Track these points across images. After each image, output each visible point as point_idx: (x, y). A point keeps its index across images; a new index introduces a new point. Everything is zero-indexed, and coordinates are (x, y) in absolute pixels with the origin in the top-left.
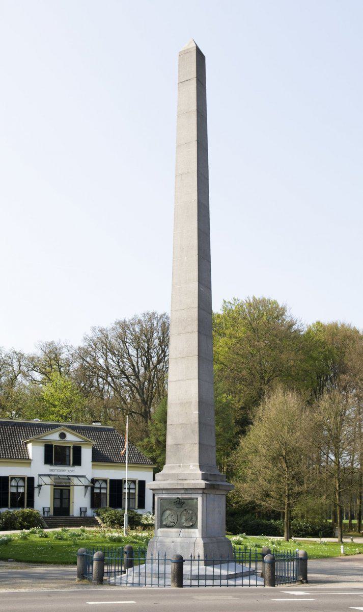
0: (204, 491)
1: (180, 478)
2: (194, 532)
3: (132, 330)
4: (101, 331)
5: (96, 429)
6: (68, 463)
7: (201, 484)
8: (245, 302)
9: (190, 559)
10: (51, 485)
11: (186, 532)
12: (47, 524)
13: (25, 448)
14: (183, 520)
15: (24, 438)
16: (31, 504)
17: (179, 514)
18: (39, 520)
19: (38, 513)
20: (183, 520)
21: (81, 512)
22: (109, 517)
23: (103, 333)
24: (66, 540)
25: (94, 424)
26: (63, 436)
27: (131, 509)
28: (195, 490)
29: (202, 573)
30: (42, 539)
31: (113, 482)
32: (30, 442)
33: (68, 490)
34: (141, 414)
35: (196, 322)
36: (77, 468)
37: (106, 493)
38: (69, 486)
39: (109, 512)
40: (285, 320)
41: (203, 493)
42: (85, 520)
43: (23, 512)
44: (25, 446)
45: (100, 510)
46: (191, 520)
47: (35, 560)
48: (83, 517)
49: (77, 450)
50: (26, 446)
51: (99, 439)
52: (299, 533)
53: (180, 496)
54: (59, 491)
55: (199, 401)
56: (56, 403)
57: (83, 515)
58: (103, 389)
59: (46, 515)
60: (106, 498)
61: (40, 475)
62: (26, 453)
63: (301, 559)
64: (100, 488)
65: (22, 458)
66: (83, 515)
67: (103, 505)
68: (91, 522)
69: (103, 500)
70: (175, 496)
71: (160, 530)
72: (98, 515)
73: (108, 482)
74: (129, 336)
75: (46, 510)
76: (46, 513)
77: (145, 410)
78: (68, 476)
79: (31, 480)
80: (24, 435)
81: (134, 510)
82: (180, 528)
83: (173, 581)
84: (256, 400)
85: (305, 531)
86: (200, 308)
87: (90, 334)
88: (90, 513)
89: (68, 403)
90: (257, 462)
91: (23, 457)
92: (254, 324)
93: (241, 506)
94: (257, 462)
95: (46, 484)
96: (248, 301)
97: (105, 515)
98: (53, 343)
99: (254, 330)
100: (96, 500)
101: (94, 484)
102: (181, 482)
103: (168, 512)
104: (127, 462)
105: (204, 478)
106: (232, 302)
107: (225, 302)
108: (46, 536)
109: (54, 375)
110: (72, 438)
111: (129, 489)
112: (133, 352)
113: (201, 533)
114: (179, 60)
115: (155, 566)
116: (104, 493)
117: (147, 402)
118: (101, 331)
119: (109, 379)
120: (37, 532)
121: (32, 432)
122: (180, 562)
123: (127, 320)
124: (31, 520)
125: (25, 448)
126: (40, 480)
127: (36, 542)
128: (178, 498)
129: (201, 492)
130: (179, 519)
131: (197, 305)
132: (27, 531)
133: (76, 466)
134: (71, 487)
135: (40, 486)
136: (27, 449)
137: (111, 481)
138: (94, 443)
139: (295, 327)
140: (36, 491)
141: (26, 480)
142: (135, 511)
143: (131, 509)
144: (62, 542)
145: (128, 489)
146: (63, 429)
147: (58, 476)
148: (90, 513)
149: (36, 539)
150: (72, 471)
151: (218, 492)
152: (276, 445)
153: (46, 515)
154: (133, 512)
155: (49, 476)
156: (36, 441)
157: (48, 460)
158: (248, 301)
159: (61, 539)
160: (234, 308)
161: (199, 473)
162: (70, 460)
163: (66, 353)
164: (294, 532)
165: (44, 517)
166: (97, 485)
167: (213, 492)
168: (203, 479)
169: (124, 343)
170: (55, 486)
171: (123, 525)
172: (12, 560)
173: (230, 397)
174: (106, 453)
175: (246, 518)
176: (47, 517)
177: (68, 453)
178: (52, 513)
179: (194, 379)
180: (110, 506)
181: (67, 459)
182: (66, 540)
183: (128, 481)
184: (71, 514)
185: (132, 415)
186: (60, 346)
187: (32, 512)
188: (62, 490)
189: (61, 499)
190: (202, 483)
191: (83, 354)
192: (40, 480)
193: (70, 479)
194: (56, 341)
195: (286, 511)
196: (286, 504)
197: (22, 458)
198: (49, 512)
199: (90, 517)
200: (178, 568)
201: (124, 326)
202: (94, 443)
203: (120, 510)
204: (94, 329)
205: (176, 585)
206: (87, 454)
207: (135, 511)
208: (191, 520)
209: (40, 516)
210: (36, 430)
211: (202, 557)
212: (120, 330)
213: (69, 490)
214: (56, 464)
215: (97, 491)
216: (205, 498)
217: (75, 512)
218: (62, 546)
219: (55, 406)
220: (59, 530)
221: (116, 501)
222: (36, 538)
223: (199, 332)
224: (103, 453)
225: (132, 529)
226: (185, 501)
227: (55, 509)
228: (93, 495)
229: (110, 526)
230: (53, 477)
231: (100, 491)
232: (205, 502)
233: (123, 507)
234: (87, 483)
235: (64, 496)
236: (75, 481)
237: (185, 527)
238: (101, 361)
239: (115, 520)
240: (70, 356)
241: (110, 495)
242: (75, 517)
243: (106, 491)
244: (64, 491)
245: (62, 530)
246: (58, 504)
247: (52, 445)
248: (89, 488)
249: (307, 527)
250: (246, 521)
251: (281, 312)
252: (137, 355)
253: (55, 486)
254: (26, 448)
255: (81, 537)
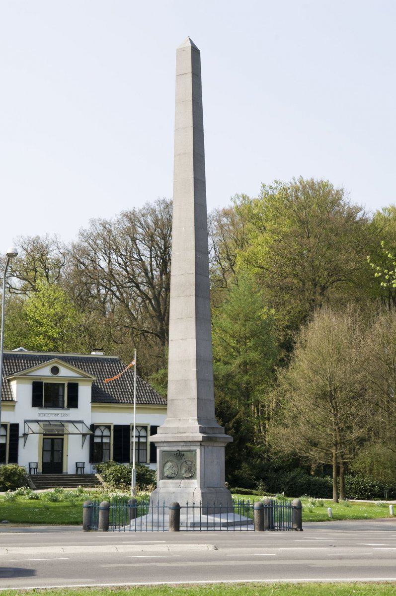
0: (202, 443)
1: (181, 431)
2: (193, 483)
3: (143, 223)
4: (103, 225)
5: (97, 360)
6: (61, 405)
7: (199, 437)
8: (290, 185)
9: (186, 506)
10: (39, 433)
11: (185, 483)
12: (34, 483)
13: (8, 387)
14: (183, 472)
15: (6, 374)
16: (14, 458)
17: (179, 466)
18: (24, 479)
19: (23, 470)
20: (183, 472)
21: (77, 468)
22: (112, 474)
23: (105, 228)
24: (62, 501)
25: (93, 353)
26: (55, 370)
27: (142, 464)
28: (193, 442)
29: (197, 520)
30: (33, 501)
31: (117, 428)
32: (14, 379)
33: (61, 440)
34: (156, 335)
35: (194, 287)
36: (72, 411)
37: (110, 443)
38: (63, 435)
39: (113, 468)
40: (81, 506)
41: (201, 445)
42: (82, 479)
43: (5, 469)
44: (7, 384)
45: (101, 465)
46: (190, 471)
47: (34, 521)
48: (80, 475)
49: (73, 388)
50: (9, 384)
51: (101, 372)
52: (362, 494)
53: (180, 449)
54: (50, 440)
55: (197, 360)
56: (44, 321)
57: (79, 473)
58: (105, 299)
59: (32, 473)
60: (110, 449)
61: (26, 422)
62: (9, 393)
63: (295, 507)
64: (102, 437)
65: (4, 399)
66: (79, 473)
67: (105, 458)
68: (91, 481)
69: (106, 453)
70: (175, 449)
71: (161, 481)
72: (99, 471)
73: (112, 428)
74: (140, 230)
75: (33, 466)
76: (33, 470)
77: (161, 329)
78: (61, 421)
79: (15, 427)
80: (7, 369)
81: (144, 464)
82: (180, 479)
83: (171, 526)
84: (302, 319)
85: (371, 490)
86: (197, 273)
87: (87, 227)
88: (88, 469)
89: (59, 320)
90: (300, 402)
91: (6, 398)
92: (303, 215)
93: (280, 458)
94: (300, 402)
95: (34, 433)
96: (293, 184)
97: (108, 472)
98: (37, 238)
99: (303, 223)
100: (96, 453)
101: (94, 432)
102: (182, 435)
103: (169, 464)
104: (135, 399)
105: (202, 431)
106: (274, 186)
107: (264, 186)
108: (37, 498)
109: (41, 283)
110: (66, 373)
111: (138, 437)
112: (145, 252)
113: (199, 483)
114: (177, 56)
115: (155, 516)
116: (106, 443)
117: (164, 317)
118: (103, 225)
119: (114, 288)
120: (25, 493)
121: (16, 366)
122: (177, 509)
123: (137, 210)
124: (16, 478)
125: (8, 387)
126: (27, 427)
127: (26, 503)
128: (178, 450)
129: (199, 444)
130: (179, 471)
131: (194, 272)
132: (13, 493)
133: (71, 409)
134: (65, 436)
135: (25, 435)
136: (10, 389)
137: (115, 426)
138: (94, 378)
139: (359, 215)
140: (21, 441)
141: (8, 427)
142: (147, 466)
143: (142, 464)
144: (58, 504)
145: (136, 437)
146: (56, 362)
147: (49, 421)
148: (88, 469)
149: (25, 501)
150: (66, 415)
151: (216, 444)
152: (320, 380)
153: (32, 473)
154: (144, 467)
155: (37, 421)
156: (21, 379)
157: (37, 402)
158: (293, 184)
159: (55, 500)
160: (276, 193)
161: (197, 426)
162: (63, 401)
163: (55, 252)
164: (356, 492)
165: (30, 475)
166: (98, 432)
167: (211, 444)
168: (200, 432)
169: (134, 240)
170: (44, 435)
171: (131, 485)
172: (7, 521)
173: (273, 311)
174: (109, 391)
175: (293, 474)
176: (34, 475)
177: (61, 393)
178: (40, 470)
179: (192, 338)
180: (115, 459)
181: (61, 399)
182: (62, 501)
183: (136, 426)
184: (64, 471)
185: (144, 335)
186: (47, 243)
187: (16, 469)
188: (53, 439)
189: (52, 451)
190: (199, 436)
191: (78, 254)
192: (27, 427)
193: (63, 426)
194: (42, 236)
195: (333, 463)
196: (334, 454)
197: (4, 399)
198: (37, 468)
199: (88, 475)
200: (175, 514)
201: (132, 217)
202: (94, 378)
203: (126, 465)
204: (93, 222)
205: (173, 529)
206: (85, 393)
207: (147, 466)
208: (190, 471)
209: (26, 474)
210: (22, 363)
211: (198, 504)
212: (128, 224)
213: (62, 439)
214: (46, 407)
215: (97, 440)
216: (203, 451)
217: (69, 468)
218: (59, 507)
219: (40, 324)
220: (52, 490)
221: (122, 454)
222: (24, 500)
223: (196, 296)
224: (105, 391)
225: (141, 489)
226: (184, 453)
227: (44, 464)
228: (93, 445)
229: (113, 486)
230: (42, 424)
231: (102, 440)
232: (203, 453)
233: (131, 461)
234: (85, 430)
235: (56, 448)
236: (70, 428)
237: (186, 478)
238: (103, 264)
239: (120, 478)
240: (61, 255)
241: (114, 445)
242: (69, 475)
243: (109, 440)
244: (55, 440)
245: (55, 490)
246: (48, 459)
247: (42, 382)
248: (88, 437)
249: (374, 486)
250: (294, 478)
251: (336, 199)
252: (151, 255)
253: (44, 435)
254: (9, 386)
255: (80, 498)
